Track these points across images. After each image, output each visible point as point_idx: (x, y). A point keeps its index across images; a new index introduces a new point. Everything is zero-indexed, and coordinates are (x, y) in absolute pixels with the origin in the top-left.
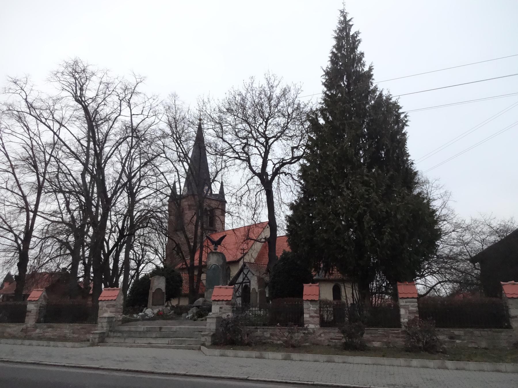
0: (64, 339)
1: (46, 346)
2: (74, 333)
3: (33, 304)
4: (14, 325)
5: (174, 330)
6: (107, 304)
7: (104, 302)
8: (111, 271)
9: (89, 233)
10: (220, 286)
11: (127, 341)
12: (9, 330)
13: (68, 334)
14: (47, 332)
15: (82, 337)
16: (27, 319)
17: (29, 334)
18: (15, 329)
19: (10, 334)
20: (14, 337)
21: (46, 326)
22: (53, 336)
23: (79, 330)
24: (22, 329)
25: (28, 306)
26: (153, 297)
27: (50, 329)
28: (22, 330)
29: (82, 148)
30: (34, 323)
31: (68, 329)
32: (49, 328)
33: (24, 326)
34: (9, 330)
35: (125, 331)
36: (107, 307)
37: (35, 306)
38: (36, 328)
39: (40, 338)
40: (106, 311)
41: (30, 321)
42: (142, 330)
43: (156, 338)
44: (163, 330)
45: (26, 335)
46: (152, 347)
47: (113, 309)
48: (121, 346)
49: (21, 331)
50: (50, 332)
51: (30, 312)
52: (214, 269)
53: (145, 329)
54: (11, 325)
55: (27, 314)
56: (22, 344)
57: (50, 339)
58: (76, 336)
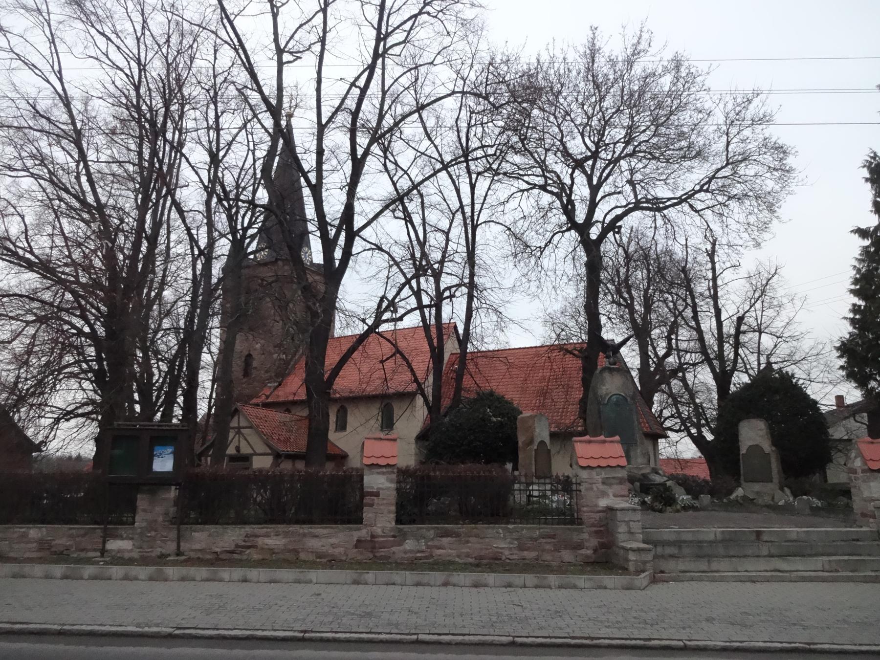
0: (492, 563)
1: (536, 587)
2: (521, 548)
3: (384, 473)
4: (325, 531)
5: (794, 536)
6: (604, 475)
7: (594, 473)
8: (136, 396)
9: (424, 303)
10: (602, 438)
11: (715, 566)
12: (314, 544)
13: (507, 553)
14: (439, 548)
15: (547, 557)
16: (368, 514)
17: (383, 552)
18: (333, 540)
19: (320, 556)
20: (332, 562)
21: (431, 534)
22: (458, 556)
23: (536, 540)
24: (359, 541)
25: (366, 479)
26: (535, 461)
27: (445, 540)
28: (359, 543)
29: (151, 102)
30: (394, 523)
31: (505, 538)
32: (442, 537)
33: (363, 533)
34: (314, 544)
35: (685, 542)
36: (603, 483)
37: (391, 481)
38: (400, 537)
39: (412, 564)
40: (604, 494)
41: (381, 519)
42: (711, 537)
43: (771, 556)
44: (765, 538)
45: (373, 558)
46: (782, 580)
47: (617, 488)
48: (700, 580)
49: (356, 546)
50: (447, 548)
51: (377, 494)
52: (617, 404)
53: (719, 537)
54: (319, 530)
55: (367, 500)
56: (446, 584)
57: (445, 565)
58: (530, 555)
